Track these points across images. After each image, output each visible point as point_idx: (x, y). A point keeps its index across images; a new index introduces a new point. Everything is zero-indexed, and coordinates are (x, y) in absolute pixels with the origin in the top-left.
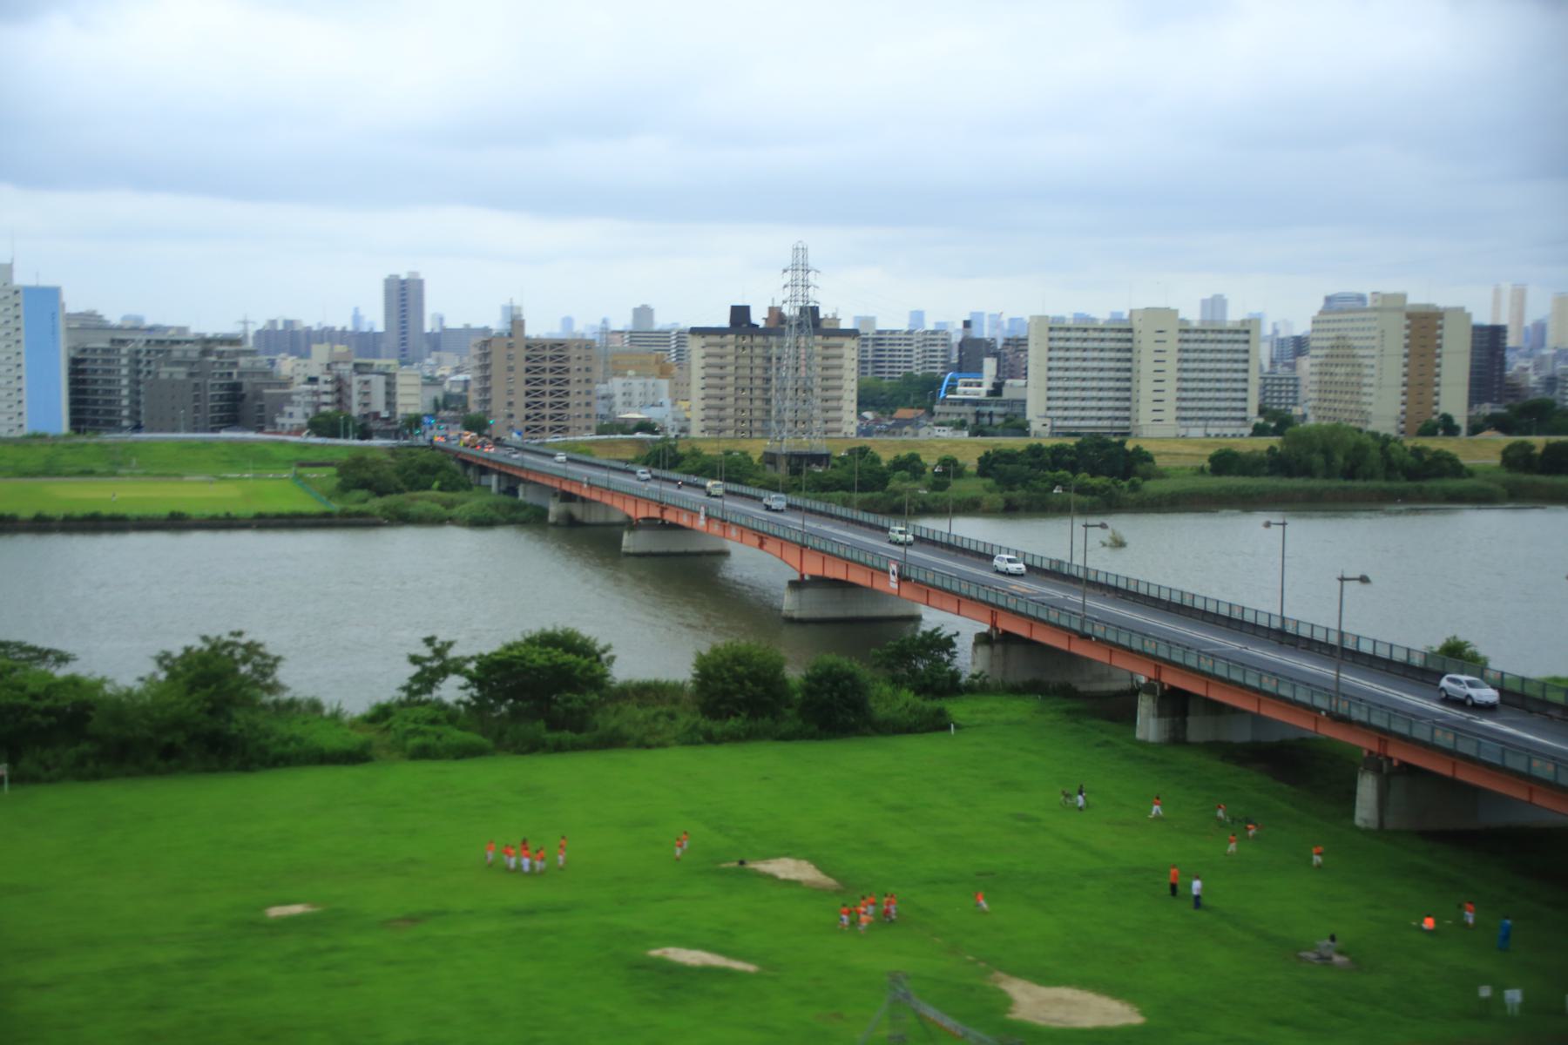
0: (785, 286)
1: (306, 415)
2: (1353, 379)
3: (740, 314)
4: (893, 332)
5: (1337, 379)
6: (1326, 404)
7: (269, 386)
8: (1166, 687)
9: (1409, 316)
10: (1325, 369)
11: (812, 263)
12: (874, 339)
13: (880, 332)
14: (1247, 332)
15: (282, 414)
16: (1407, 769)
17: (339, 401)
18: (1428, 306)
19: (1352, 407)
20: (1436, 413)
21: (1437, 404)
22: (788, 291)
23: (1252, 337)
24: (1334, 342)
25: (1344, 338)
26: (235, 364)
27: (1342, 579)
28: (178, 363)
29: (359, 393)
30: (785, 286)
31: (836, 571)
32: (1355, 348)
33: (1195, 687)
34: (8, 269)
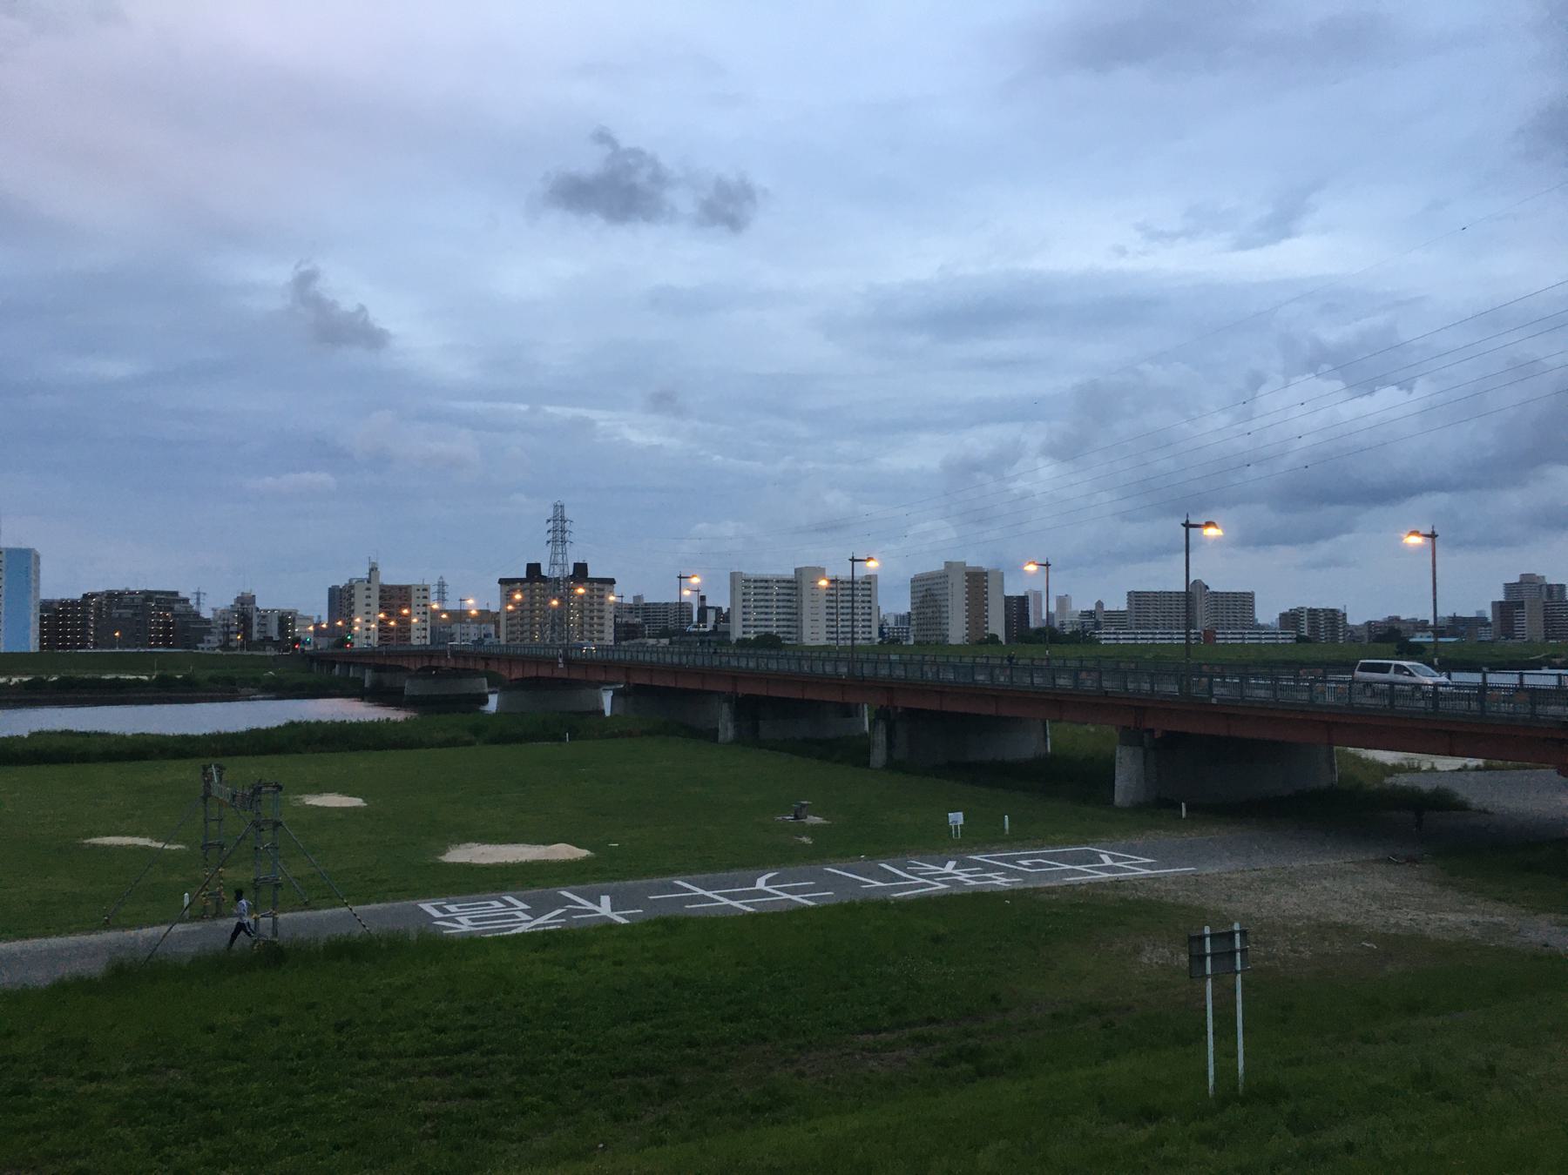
0: (549, 531)
1: (220, 641)
2: (937, 615)
3: (533, 569)
4: (655, 604)
5: (928, 615)
6: (922, 633)
7: (195, 623)
8: (740, 696)
9: (967, 574)
10: (920, 610)
11: (567, 516)
12: (643, 609)
13: (646, 604)
14: (869, 583)
15: (202, 641)
16: (913, 714)
17: (244, 629)
18: (978, 568)
19: (938, 632)
20: (987, 634)
21: (987, 628)
22: (551, 535)
23: (873, 586)
24: (924, 593)
25: (930, 589)
26: (171, 609)
27: (853, 560)
28: (125, 607)
29: (258, 624)
30: (549, 531)
31: (532, 672)
32: (936, 595)
33: (760, 690)
34: (23, 562)
